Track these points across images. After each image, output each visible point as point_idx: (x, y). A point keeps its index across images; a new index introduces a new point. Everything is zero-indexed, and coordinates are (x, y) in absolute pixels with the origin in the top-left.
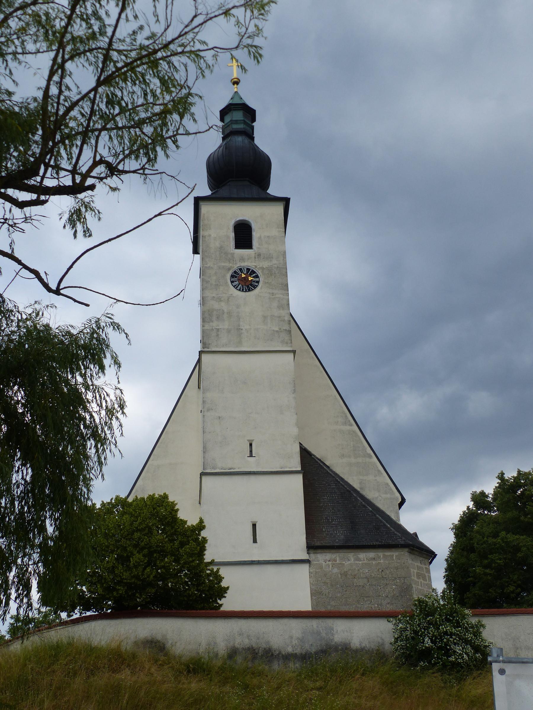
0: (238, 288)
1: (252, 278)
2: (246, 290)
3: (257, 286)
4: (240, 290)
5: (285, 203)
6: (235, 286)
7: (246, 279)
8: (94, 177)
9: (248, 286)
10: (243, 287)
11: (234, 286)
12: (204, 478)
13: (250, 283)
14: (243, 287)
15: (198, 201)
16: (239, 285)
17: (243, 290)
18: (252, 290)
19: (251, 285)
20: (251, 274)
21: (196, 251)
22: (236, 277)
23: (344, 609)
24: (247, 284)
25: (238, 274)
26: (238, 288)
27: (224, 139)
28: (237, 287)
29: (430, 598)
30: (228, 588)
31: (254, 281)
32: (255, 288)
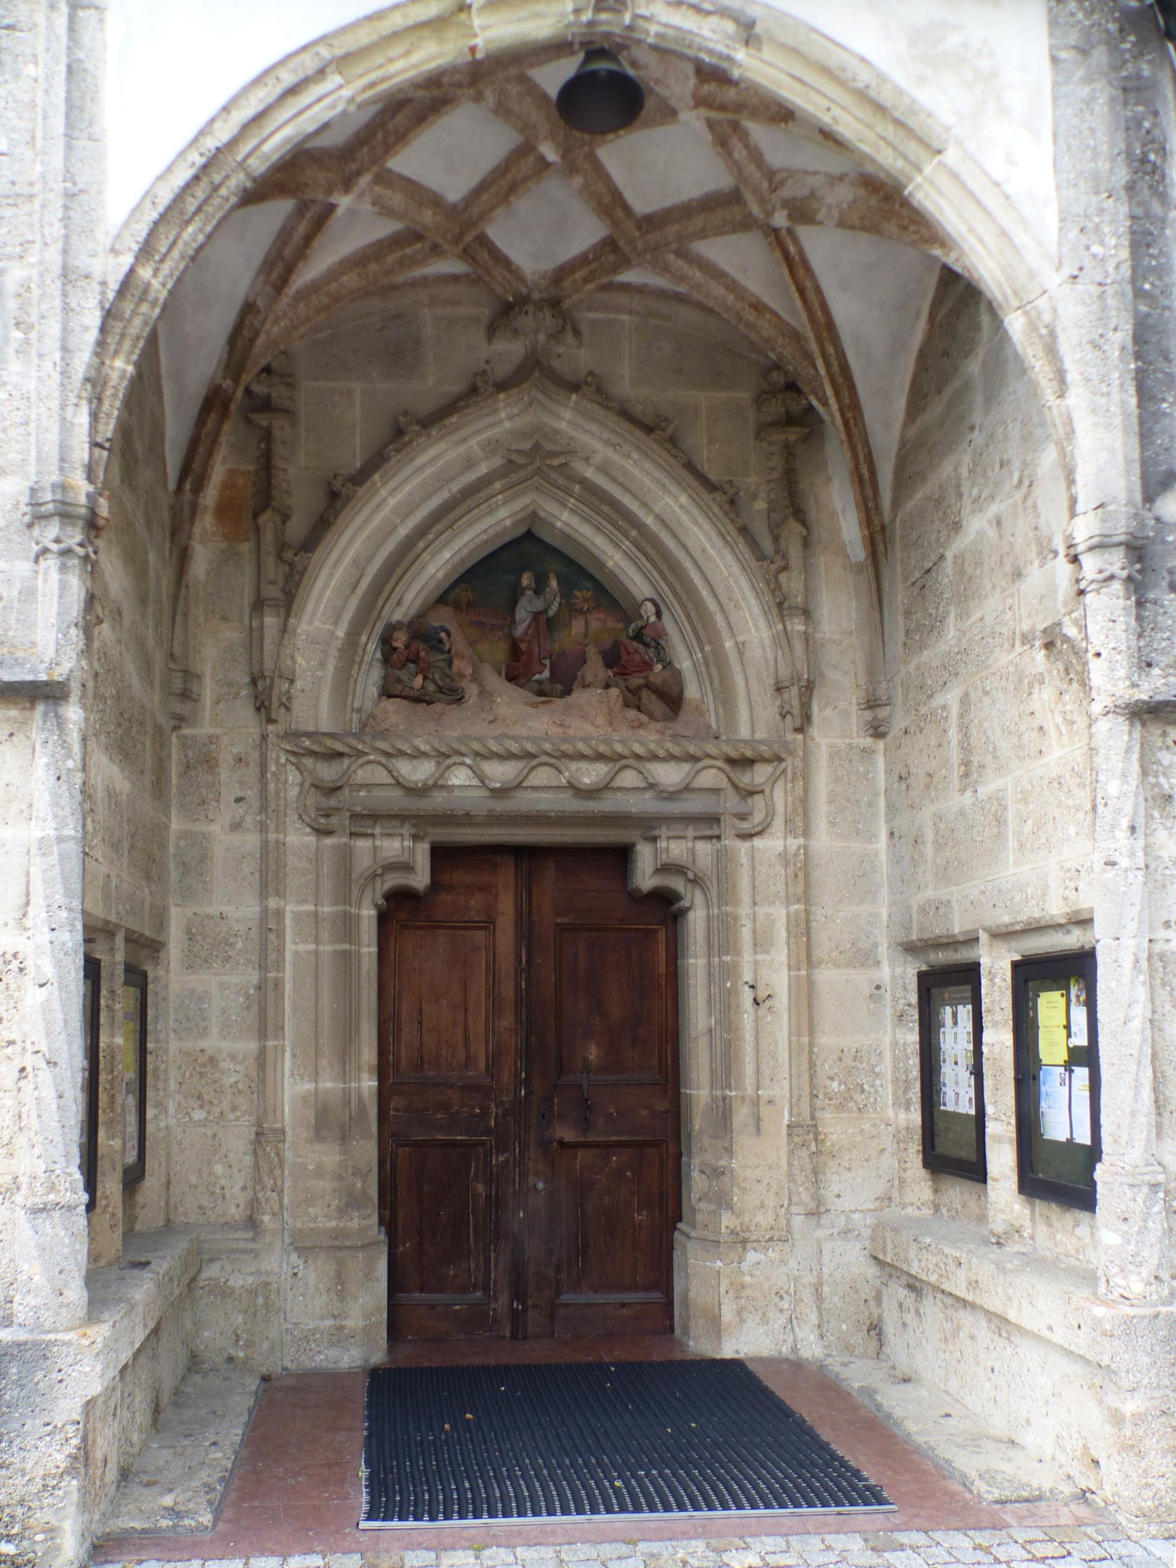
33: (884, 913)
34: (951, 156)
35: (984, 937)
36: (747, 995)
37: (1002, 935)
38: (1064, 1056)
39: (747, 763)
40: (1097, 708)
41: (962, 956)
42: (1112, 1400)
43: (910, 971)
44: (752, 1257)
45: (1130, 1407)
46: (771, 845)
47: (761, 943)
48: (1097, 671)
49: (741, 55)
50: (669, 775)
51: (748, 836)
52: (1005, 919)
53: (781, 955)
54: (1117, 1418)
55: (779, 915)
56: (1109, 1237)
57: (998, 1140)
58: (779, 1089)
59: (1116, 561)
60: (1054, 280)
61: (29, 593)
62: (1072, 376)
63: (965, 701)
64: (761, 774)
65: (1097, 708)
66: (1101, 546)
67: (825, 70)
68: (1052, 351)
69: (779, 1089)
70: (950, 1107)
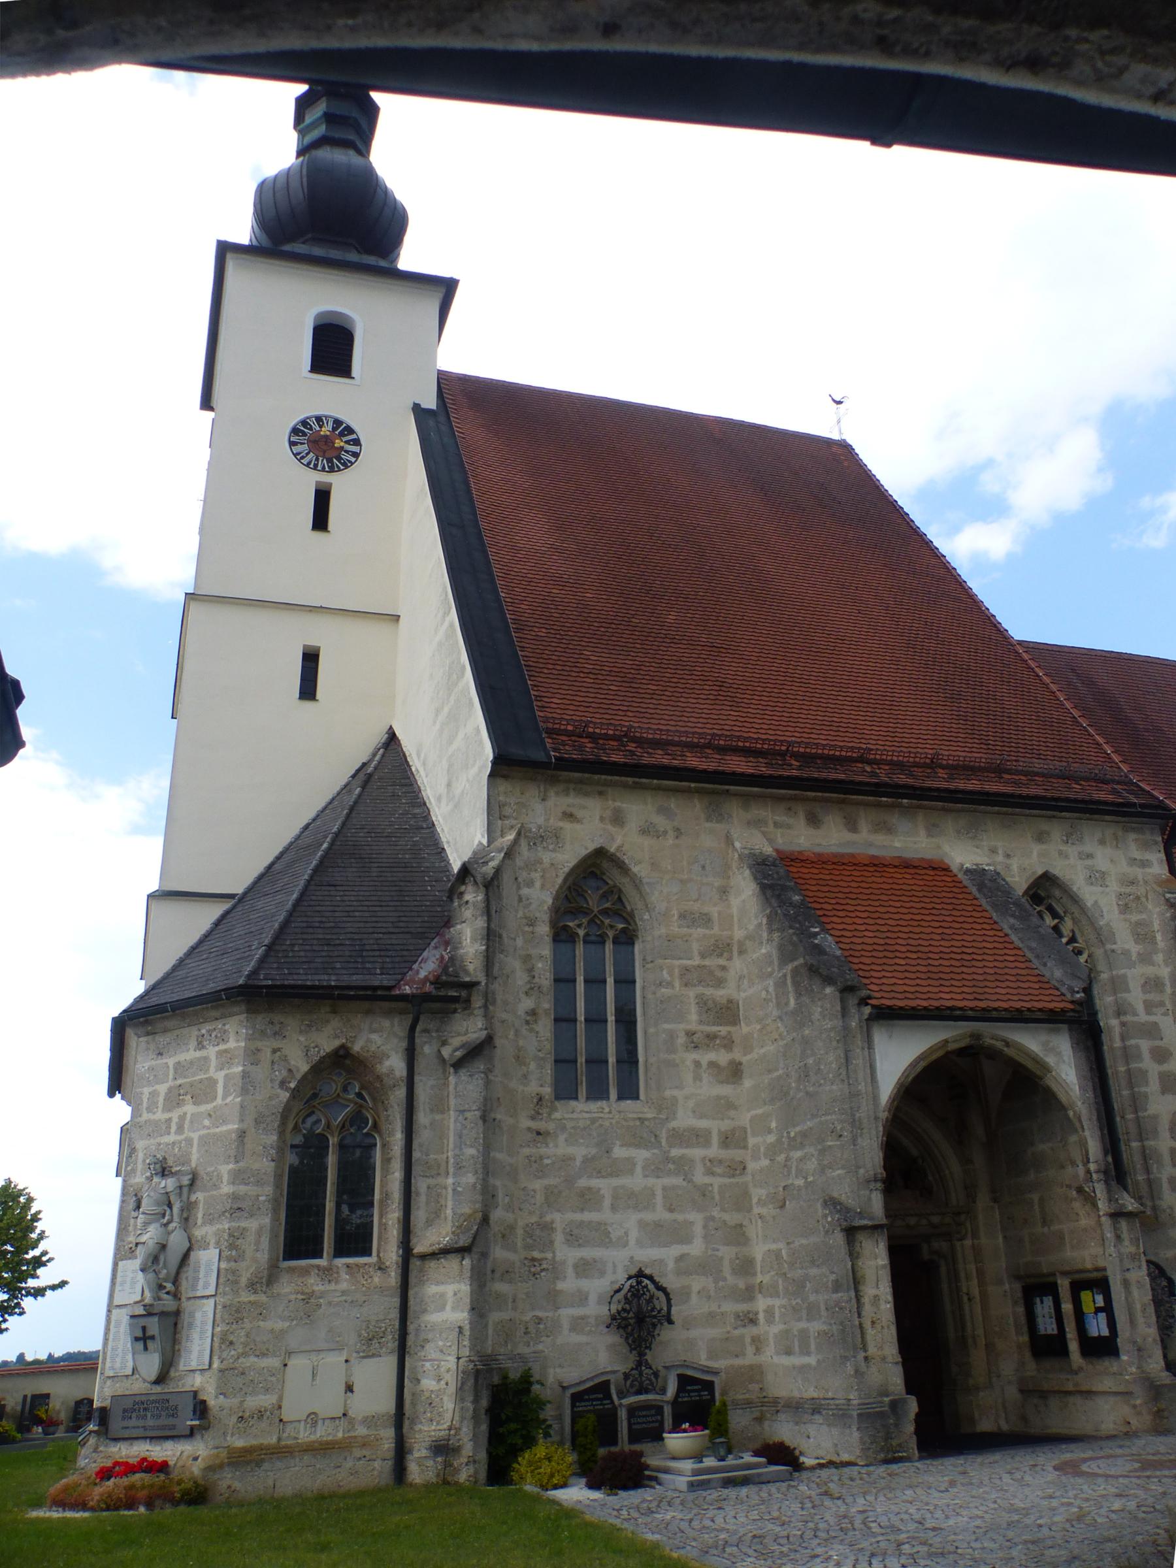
0: (305, 461)
1: (342, 444)
2: (324, 467)
3: (352, 464)
4: (308, 465)
5: (444, 291)
6: (298, 454)
7: (327, 440)
8: (208, 1297)
9: (330, 461)
10: (317, 459)
11: (295, 455)
12: (194, 607)
13: (335, 454)
14: (317, 459)
15: (225, 250)
16: (307, 454)
17: (316, 466)
18: (340, 470)
19: (339, 458)
20: (342, 434)
21: (207, 403)
22: (304, 434)
23: (415, 1145)
24: (327, 455)
25: (311, 429)
26: (305, 461)
27: (300, 153)
28: (303, 458)
29: (1045, 1223)
30: (38, 1277)
31: (347, 452)
32: (347, 467)
33: (1004, 1265)
34: (1054, 1073)
35: (1058, 1274)
36: (965, 1298)
37: (1065, 1274)
38: (1093, 1310)
39: (959, 1214)
40: (1101, 1213)
41: (1051, 1279)
42: (1132, 1402)
43: (1018, 1286)
44: (981, 1394)
45: (1138, 1402)
46: (968, 1242)
47: (968, 1278)
48: (1100, 1204)
49: (1005, 1049)
50: (936, 1219)
51: (961, 1240)
52: (1067, 1268)
53: (975, 1282)
54: (1135, 1407)
55: (972, 1268)
56: (1124, 1358)
57: (1071, 1339)
58: (980, 1332)
59: (1102, 1176)
60: (1079, 1103)
61: (870, 1199)
62: (1085, 1127)
63: (1041, 1200)
64: (963, 1217)
65: (1101, 1213)
66: (1097, 1172)
67: (1025, 1053)
68: (1080, 1120)
69: (980, 1332)
70: (1042, 1332)
